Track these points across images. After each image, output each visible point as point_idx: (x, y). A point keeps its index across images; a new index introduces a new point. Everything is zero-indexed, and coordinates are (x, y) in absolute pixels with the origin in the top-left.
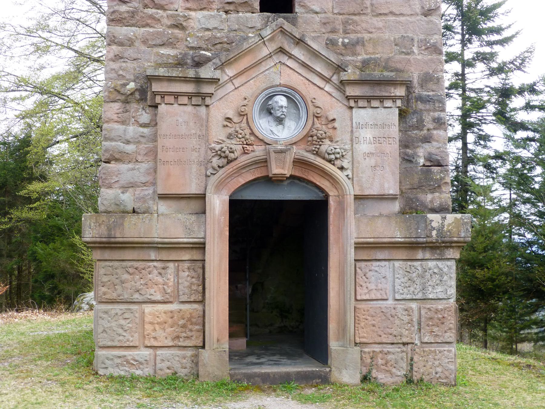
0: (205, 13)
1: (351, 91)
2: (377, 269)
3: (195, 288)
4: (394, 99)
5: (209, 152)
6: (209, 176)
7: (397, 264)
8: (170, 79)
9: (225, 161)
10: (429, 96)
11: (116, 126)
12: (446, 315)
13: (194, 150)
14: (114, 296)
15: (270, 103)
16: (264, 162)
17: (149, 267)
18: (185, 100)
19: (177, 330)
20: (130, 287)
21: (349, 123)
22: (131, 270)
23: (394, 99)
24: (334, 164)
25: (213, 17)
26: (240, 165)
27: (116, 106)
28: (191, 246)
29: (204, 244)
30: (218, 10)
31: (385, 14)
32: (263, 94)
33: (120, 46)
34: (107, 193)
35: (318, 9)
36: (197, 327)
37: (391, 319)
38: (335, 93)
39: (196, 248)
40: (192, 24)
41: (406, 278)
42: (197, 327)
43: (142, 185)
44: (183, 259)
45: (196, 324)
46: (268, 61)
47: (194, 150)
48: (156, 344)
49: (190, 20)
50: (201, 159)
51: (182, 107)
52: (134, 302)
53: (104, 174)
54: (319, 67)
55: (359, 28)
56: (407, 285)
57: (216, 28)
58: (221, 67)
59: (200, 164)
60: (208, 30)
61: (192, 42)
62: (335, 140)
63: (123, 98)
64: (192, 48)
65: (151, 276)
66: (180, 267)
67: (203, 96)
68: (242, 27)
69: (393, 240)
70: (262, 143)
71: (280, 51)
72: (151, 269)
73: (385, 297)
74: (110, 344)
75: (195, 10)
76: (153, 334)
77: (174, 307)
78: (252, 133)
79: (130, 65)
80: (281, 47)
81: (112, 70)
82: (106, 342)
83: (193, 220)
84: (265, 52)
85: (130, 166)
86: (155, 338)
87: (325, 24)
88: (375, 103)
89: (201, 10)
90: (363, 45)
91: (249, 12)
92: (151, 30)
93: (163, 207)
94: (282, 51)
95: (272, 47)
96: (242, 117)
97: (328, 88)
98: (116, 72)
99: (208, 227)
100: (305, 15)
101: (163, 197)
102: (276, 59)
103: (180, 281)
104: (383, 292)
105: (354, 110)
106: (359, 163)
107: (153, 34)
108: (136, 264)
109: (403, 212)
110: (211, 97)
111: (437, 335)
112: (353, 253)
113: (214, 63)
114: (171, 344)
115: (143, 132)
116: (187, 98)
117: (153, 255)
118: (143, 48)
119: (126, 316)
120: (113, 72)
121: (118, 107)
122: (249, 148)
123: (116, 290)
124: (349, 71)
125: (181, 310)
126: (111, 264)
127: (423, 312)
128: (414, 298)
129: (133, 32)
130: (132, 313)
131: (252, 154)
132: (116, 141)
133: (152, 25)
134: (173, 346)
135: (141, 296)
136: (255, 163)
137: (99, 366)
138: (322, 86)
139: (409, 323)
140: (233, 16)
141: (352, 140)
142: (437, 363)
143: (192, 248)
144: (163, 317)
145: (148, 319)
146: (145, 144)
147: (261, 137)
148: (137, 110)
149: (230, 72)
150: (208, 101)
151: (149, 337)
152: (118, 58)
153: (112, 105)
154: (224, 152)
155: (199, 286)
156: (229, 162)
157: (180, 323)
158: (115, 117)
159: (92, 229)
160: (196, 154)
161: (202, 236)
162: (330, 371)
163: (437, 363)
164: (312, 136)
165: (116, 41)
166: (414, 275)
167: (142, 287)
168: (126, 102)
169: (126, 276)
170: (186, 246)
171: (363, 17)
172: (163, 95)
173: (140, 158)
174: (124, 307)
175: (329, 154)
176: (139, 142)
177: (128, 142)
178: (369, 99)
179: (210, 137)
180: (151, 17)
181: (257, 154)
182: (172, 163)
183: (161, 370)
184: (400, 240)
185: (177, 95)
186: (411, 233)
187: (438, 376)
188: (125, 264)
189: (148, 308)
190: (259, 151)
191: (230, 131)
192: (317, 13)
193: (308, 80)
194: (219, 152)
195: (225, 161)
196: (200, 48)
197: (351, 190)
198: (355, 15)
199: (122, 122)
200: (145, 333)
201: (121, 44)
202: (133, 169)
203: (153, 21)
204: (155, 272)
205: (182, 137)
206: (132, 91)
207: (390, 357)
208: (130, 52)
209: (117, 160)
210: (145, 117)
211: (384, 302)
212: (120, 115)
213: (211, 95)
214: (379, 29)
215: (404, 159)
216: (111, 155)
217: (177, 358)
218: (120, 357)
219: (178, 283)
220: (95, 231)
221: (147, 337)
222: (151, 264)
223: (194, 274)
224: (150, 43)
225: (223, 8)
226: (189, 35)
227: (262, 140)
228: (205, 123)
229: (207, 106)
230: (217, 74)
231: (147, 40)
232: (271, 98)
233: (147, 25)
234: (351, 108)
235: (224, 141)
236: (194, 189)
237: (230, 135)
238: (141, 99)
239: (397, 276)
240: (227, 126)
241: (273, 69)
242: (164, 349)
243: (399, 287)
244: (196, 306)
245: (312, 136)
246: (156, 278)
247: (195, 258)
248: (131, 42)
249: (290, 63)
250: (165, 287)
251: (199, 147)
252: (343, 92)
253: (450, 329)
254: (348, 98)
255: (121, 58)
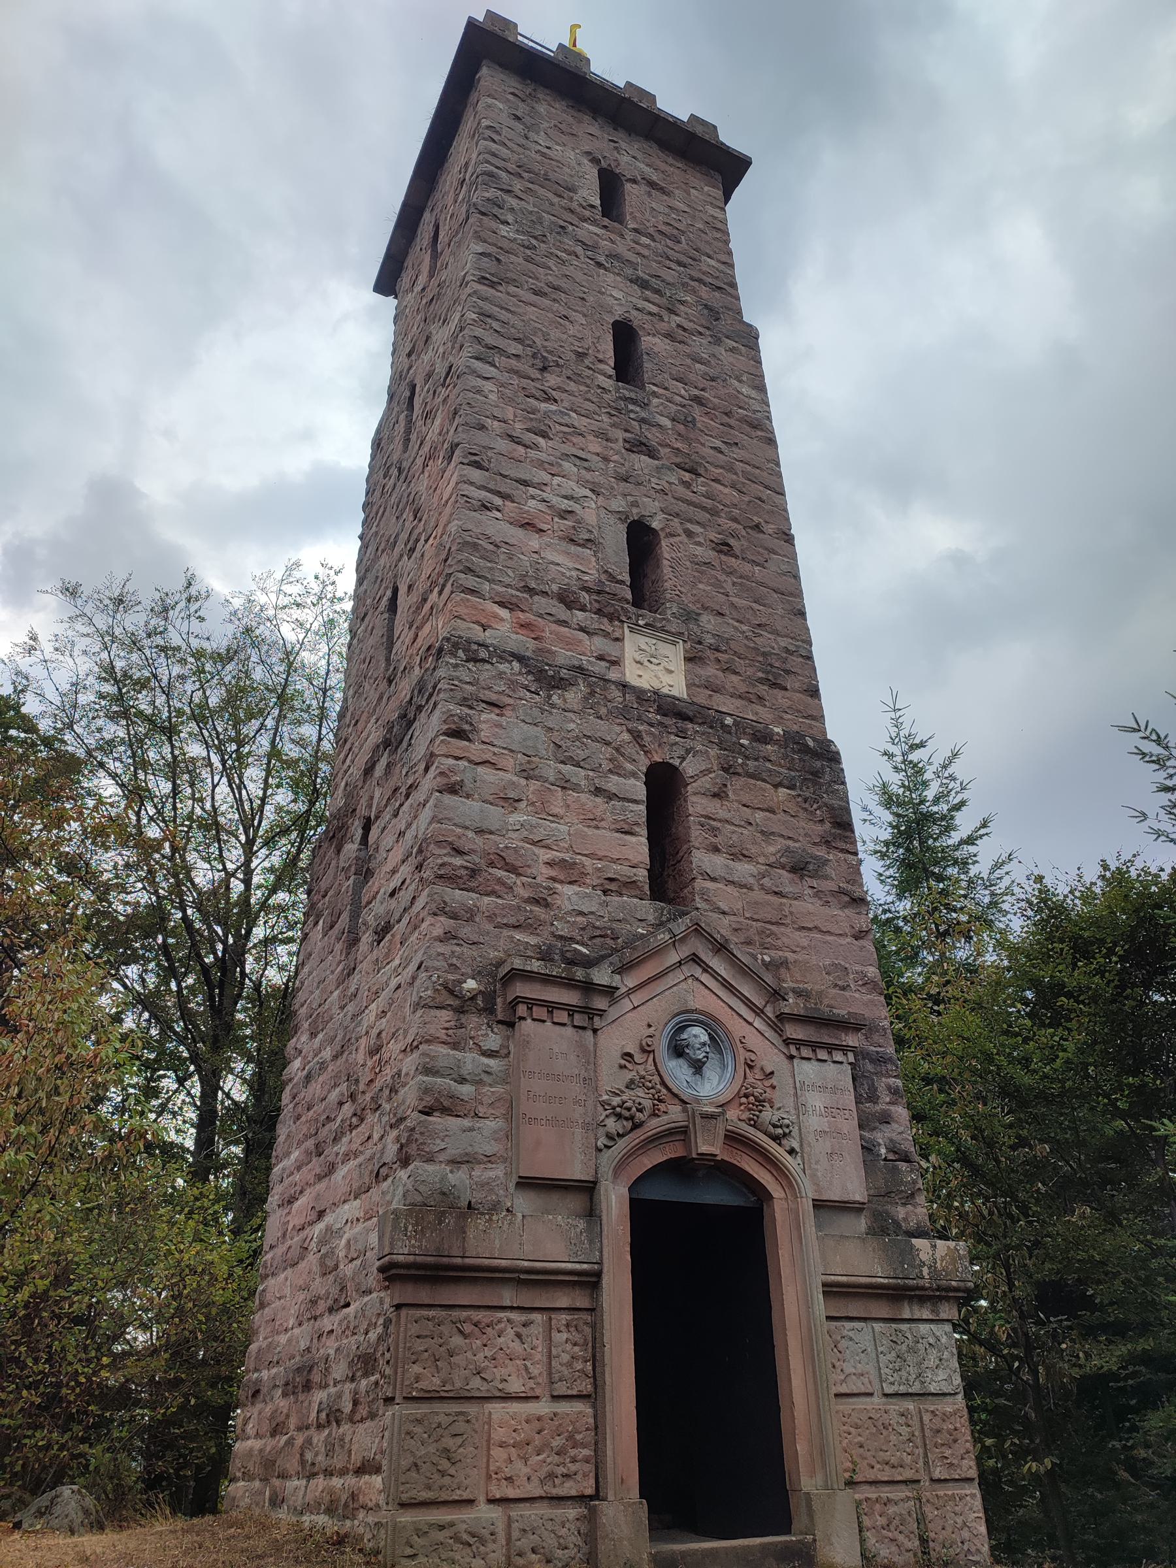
0: (576, 888)
1: (794, 1032)
2: (851, 1334)
3: (579, 1366)
4: (844, 1049)
5: (600, 1108)
6: (600, 1150)
7: (878, 1326)
8: (546, 980)
9: (629, 1125)
10: (877, 1052)
11: (443, 1050)
12: (958, 1425)
13: (576, 1102)
14: (433, 1382)
15: (684, 1036)
16: (681, 1133)
17: (499, 1322)
18: (562, 1016)
19: (549, 1460)
20: (463, 1364)
21: (791, 1081)
22: (467, 1328)
23: (844, 1049)
24: (780, 1144)
25: (587, 895)
26: (650, 1134)
27: (445, 1015)
28: (576, 1278)
29: (598, 1274)
30: (594, 887)
31: (810, 929)
32: (677, 1019)
33: (451, 918)
34: (425, 1171)
35: (726, 909)
36: (586, 1452)
37: (884, 1431)
38: (769, 1033)
39: (574, 1283)
40: (559, 902)
41: (893, 1354)
42: (586, 1452)
43: (486, 1159)
44: (558, 1306)
45: (584, 1446)
46: (678, 971)
47: (576, 1102)
48: (511, 1493)
49: (555, 896)
50: (588, 1120)
51: (558, 1028)
52: (472, 1398)
53: (422, 1133)
54: (746, 990)
55: (779, 943)
56: (897, 1366)
57: (592, 913)
58: (622, 970)
59: (586, 1126)
60: (581, 913)
61: (562, 929)
62: (777, 1105)
63: (457, 1002)
64: (561, 937)
65: (502, 1340)
66: (553, 1322)
67: (591, 1013)
68: (628, 918)
69: (874, 1280)
70: (677, 1101)
71: (693, 960)
72: (503, 1325)
73: (870, 1391)
74: (425, 1495)
75: (562, 882)
76: (508, 1472)
77: (543, 1408)
78: (663, 1083)
79: (466, 950)
80: (694, 954)
81: (439, 954)
82: (415, 1491)
83: (581, 1227)
84: (673, 957)
85: (466, 1123)
86: (509, 1479)
87: (736, 930)
88: (822, 1054)
89: (570, 883)
90: (788, 969)
91: (636, 897)
92: (500, 901)
93: (523, 1203)
94: (695, 959)
95: (684, 951)
96: (646, 1055)
97: (758, 1023)
98: (446, 960)
99: (605, 1241)
100: (710, 914)
101: (527, 1184)
102: (687, 970)
103: (554, 1352)
104: (866, 1381)
105: (796, 1061)
106: (809, 1145)
107: (504, 907)
108: (478, 1315)
109: (871, 1232)
110: (601, 1016)
111: (951, 1464)
112: (822, 1307)
113: (611, 963)
114: (538, 1492)
115: (488, 1066)
116: (566, 1013)
117: (507, 1296)
118: (489, 927)
119: (455, 1429)
120: (441, 958)
121: (447, 1019)
122: (662, 1107)
123: (438, 1370)
124: (791, 1001)
125: (555, 1414)
126: (431, 1313)
127: (926, 1418)
128: (910, 1391)
129: (472, 899)
130: (468, 1421)
131: (665, 1118)
132: (442, 1076)
133: (500, 893)
134: (541, 1498)
135: (485, 1383)
136: (671, 1132)
137: (398, 1552)
138: (751, 1020)
139: (909, 1440)
140: (615, 899)
141: (796, 1108)
142: (959, 1520)
143: (574, 1283)
144: (526, 1432)
145: (499, 1434)
146: (490, 1085)
147: (675, 1090)
148: (478, 1028)
149: (631, 981)
150: (597, 1021)
151: (499, 1476)
152: (449, 936)
153: (438, 1013)
154: (629, 1109)
155: (586, 1361)
156: (636, 1126)
157: (554, 1444)
158: (442, 1034)
159: (409, 1238)
160: (581, 1110)
161: (597, 1259)
162: (815, 1540)
163: (959, 1520)
164: (746, 1096)
165: (447, 909)
166: (904, 1347)
167: (487, 1363)
168: (460, 1011)
169: (457, 1340)
170: (567, 1278)
171: (782, 929)
172: (531, 1003)
173: (481, 1110)
174: (454, 1407)
175: (775, 1126)
176: (480, 1082)
177: (462, 1080)
178: (814, 1046)
179: (600, 1084)
180: (500, 881)
181: (674, 1117)
182: (543, 1122)
183: (520, 1555)
184: (882, 1280)
185: (551, 1007)
186: (895, 1270)
187: (966, 1547)
188: (455, 1314)
189: (497, 1410)
190: (674, 1114)
191: (629, 1075)
192: (724, 913)
193: (731, 1008)
194: (618, 1109)
195: (629, 1125)
196: (572, 939)
197: (809, 1191)
198: (773, 924)
199: (454, 1044)
200: (491, 1468)
201: (454, 916)
202: (471, 1129)
203: (503, 888)
204: (510, 1332)
205: (558, 1077)
206: (474, 993)
207: (892, 1510)
208: (466, 931)
209: (446, 1111)
210: (493, 1041)
211: (868, 1399)
212: (450, 1032)
213: (601, 1013)
214: (803, 948)
215: (863, 1147)
216: (437, 1100)
217: (549, 1525)
218: (442, 1527)
219: (550, 1356)
220: (413, 1242)
221: (494, 1476)
222: (501, 1315)
223: (577, 1337)
224: (499, 920)
225: (602, 885)
226: (556, 918)
227: (676, 1096)
228: (592, 1060)
229: (595, 1031)
230: (616, 980)
231: (495, 915)
232: (681, 1029)
233: (493, 893)
234: (791, 1057)
235: (623, 1092)
236: (577, 1171)
237: (632, 1081)
238: (485, 1010)
239: (880, 1349)
240: (625, 1067)
241: (683, 985)
242: (522, 1505)
243: (887, 1371)
244: (579, 1407)
245: (746, 1096)
246: (512, 1345)
247: (578, 1305)
248: (470, 915)
249: (705, 978)
250: (528, 1363)
251: (584, 1097)
252: (779, 1031)
253: (968, 1452)
254: (787, 1042)
255: (455, 938)
